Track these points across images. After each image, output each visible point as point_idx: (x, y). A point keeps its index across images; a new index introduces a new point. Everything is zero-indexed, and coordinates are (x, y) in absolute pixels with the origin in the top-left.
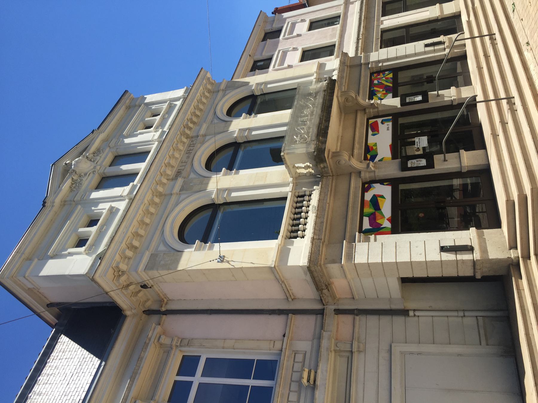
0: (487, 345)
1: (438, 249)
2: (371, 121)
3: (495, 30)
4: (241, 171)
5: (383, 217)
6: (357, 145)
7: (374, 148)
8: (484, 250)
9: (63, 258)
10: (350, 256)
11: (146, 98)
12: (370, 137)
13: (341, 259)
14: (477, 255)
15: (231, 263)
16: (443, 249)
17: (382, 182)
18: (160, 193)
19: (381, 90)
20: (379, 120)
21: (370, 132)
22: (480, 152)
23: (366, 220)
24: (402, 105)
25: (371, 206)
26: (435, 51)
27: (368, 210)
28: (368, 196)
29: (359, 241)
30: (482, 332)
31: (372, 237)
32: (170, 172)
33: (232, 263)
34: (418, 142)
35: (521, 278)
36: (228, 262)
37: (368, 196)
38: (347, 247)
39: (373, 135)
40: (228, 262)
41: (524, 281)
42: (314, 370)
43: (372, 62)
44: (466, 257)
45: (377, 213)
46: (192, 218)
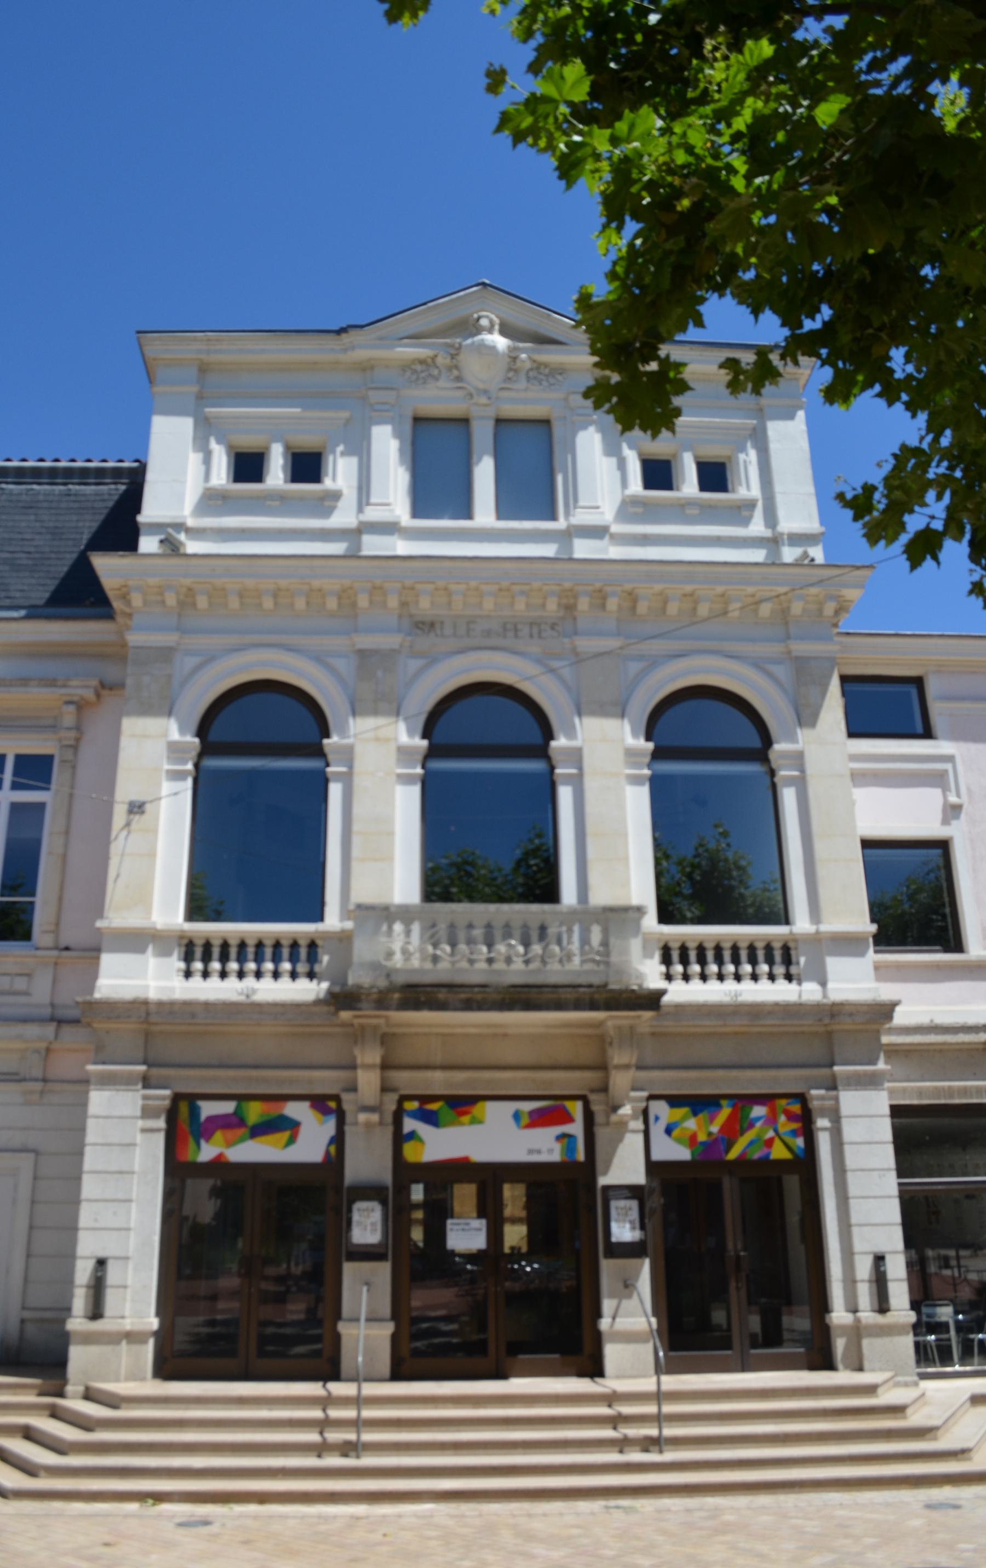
0: (23, 1321)
1: (101, 1254)
2: (576, 1109)
3: (369, 1461)
4: (644, 792)
5: (229, 1144)
6: (460, 1076)
7: (466, 1119)
8: (89, 1339)
9: (195, 438)
10: (108, 1081)
11: (914, 416)
12: (510, 1107)
13: (104, 1063)
14: (77, 1323)
15: (124, 833)
16: (879, 1259)
17: (339, 1140)
18: (354, 605)
19: (715, 1128)
20: (576, 1128)
21: (527, 1106)
22: (384, 1363)
23: (228, 1107)
24: (606, 1188)
25: (266, 1118)
26: (850, 1281)
27: (254, 1112)
28: (295, 1110)
29: (145, 1098)
30: (48, 1315)
31: (161, 1123)
32: (424, 606)
33: (124, 833)
34: (467, 1227)
35: (41, 1394)
36: (128, 824)
37: (296, 1110)
38: (130, 1073)
39: (517, 1116)
40: (128, 824)
41: (31, 1398)
42: (884, 1024)
43: (837, 1099)
44: (79, 1303)
45: (243, 1131)
46: (727, 703)
